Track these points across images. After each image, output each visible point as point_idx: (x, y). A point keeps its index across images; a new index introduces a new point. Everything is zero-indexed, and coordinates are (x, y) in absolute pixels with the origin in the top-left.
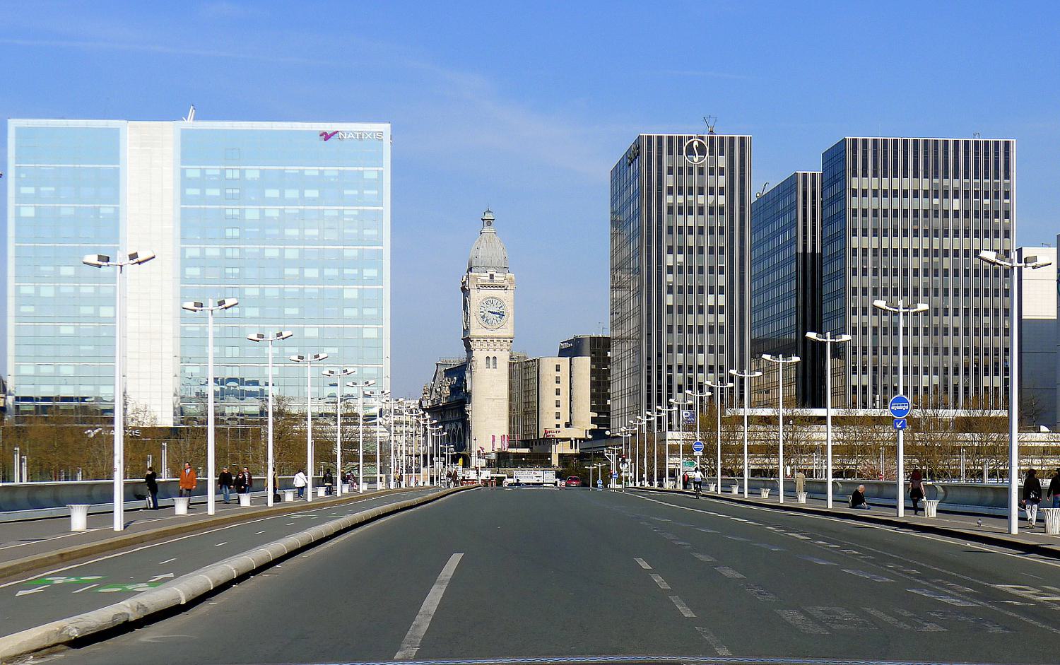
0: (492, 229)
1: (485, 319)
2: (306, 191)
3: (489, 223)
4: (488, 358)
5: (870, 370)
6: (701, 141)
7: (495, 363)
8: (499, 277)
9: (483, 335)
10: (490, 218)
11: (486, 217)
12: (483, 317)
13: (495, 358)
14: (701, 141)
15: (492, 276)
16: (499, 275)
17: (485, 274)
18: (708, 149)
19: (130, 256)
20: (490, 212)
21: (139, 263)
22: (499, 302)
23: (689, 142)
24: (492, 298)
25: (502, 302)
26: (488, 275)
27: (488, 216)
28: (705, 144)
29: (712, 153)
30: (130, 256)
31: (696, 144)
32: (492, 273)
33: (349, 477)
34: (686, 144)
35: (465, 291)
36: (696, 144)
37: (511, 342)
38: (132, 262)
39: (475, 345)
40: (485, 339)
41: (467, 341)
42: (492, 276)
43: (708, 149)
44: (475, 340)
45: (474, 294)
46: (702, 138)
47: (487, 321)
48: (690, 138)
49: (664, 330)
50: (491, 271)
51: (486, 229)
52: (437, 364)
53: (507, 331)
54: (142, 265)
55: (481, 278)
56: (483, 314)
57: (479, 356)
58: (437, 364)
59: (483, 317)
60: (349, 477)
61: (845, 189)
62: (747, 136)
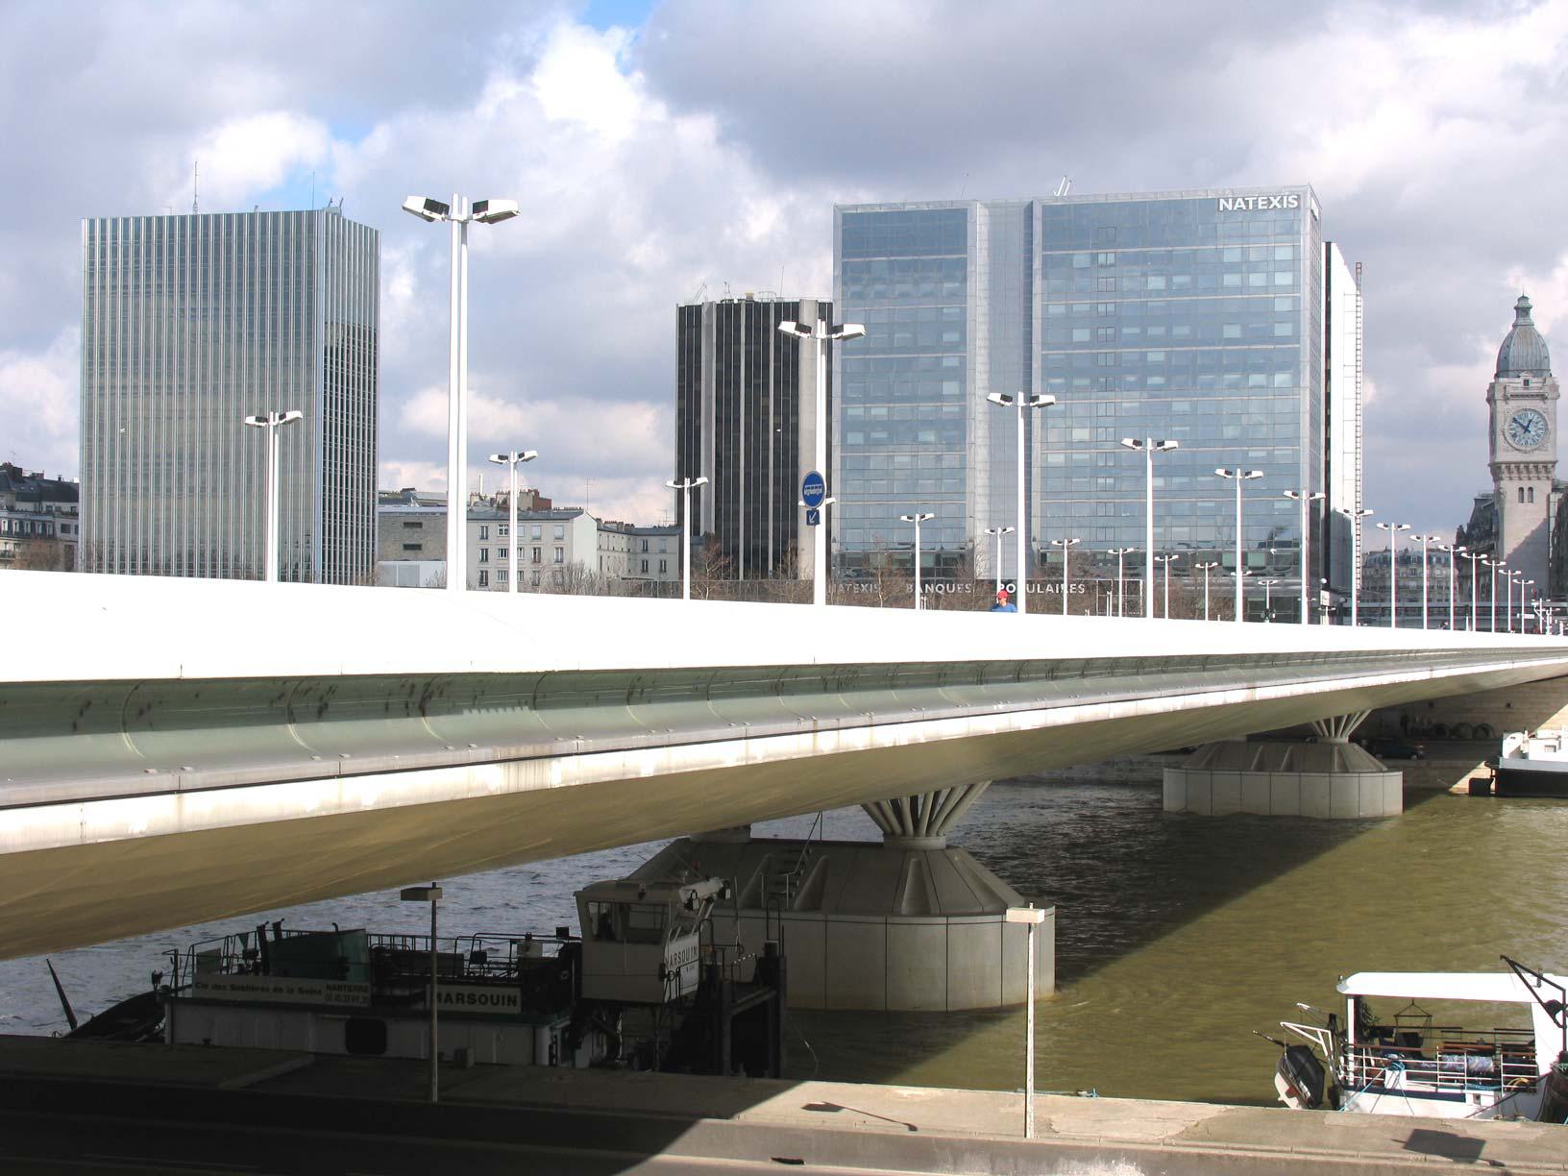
2: (1226, 276)
4: (1521, 489)
9: (1524, 460)
13: (1531, 489)
15: (1526, 382)
17: (1517, 380)
24: (1526, 410)
26: (1521, 380)
32: (1527, 378)
40: (1517, 464)
42: (1526, 382)
45: (1500, 405)
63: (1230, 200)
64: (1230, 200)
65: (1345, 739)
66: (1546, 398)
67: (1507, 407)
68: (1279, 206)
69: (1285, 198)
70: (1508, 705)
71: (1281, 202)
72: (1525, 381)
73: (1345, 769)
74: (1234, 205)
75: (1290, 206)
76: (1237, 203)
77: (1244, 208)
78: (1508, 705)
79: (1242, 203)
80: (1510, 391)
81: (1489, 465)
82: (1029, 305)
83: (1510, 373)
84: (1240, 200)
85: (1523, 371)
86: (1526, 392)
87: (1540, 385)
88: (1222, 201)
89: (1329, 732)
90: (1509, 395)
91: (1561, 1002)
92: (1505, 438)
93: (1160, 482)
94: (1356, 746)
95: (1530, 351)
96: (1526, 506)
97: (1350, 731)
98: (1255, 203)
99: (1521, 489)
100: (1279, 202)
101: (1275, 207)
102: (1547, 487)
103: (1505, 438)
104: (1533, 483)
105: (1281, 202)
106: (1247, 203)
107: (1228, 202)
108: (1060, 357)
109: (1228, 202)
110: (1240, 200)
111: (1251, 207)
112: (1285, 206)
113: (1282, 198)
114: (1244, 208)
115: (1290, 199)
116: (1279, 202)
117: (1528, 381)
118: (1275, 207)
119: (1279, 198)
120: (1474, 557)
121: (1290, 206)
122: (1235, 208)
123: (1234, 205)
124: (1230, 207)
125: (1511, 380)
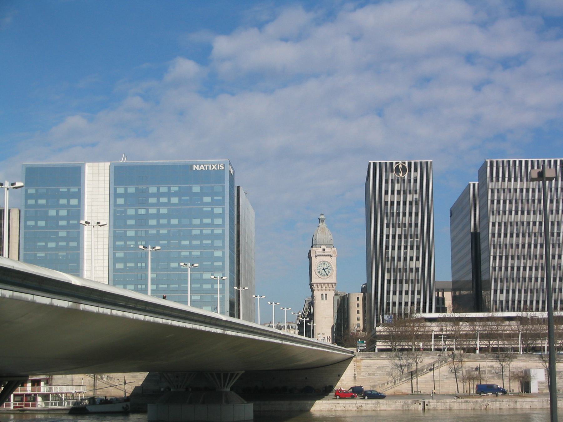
0: (324, 224)
1: (320, 273)
3: (322, 220)
4: (322, 294)
5: (504, 291)
6: (404, 164)
7: (326, 297)
8: (328, 250)
9: (319, 282)
10: (323, 218)
11: (320, 218)
12: (319, 272)
13: (326, 294)
14: (404, 164)
15: (324, 250)
16: (327, 249)
17: (320, 249)
18: (407, 169)
19: (359, 311)
20: (323, 215)
21: (101, 226)
22: (328, 264)
23: (396, 165)
24: (324, 261)
25: (329, 263)
26: (322, 249)
27: (322, 217)
28: (406, 166)
29: (410, 171)
30: (359, 311)
31: (400, 166)
32: (324, 248)
33: (377, 405)
34: (395, 166)
35: (310, 257)
36: (400, 166)
37: (335, 285)
38: (97, 225)
39: (315, 288)
40: (321, 284)
41: (311, 285)
42: (324, 250)
43: (407, 169)
44: (315, 285)
45: (313, 259)
46: (404, 163)
47: (321, 274)
48: (397, 163)
49: (385, 271)
50: (323, 247)
51: (321, 224)
52: (305, 300)
53: (333, 279)
54: (102, 227)
55: (318, 251)
56: (319, 270)
57: (318, 294)
58: (305, 300)
59: (319, 272)
60: (377, 405)
61: (487, 189)
62: (430, 161)
63: (198, 166)
64: (198, 166)
65: (229, 390)
66: (332, 256)
67: (316, 260)
68: (216, 169)
69: (218, 165)
70: (306, 378)
71: (217, 167)
72: (323, 249)
73: (227, 402)
74: (199, 168)
75: (220, 169)
76: (201, 167)
77: (204, 169)
78: (306, 378)
79: (203, 167)
80: (317, 253)
81: (309, 284)
82: (238, 220)
83: (317, 246)
84: (202, 166)
85: (322, 245)
86: (323, 254)
87: (330, 251)
88: (194, 166)
89: (221, 386)
90: (317, 255)
91: (503, 387)
92: (316, 273)
93: (154, 287)
94: (233, 392)
95: (325, 236)
96: (324, 301)
97: (231, 384)
98: (208, 167)
99: (322, 294)
100: (216, 167)
101: (214, 165)
102: (333, 294)
103: (316, 273)
104: (328, 292)
105: (217, 167)
106: (205, 167)
107: (197, 166)
108: (121, 232)
109: (197, 166)
110: (202, 166)
111: (206, 169)
112: (218, 169)
113: (217, 165)
114: (204, 169)
115: (221, 166)
116: (216, 167)
117: (324, 249)
118: (214, 165)
119: (216, 165)
120: (305, 319)
121: (220, 169)
122: (200, 169)
123: (199, 168)
124: (198, 169)
125: (317, 249)
